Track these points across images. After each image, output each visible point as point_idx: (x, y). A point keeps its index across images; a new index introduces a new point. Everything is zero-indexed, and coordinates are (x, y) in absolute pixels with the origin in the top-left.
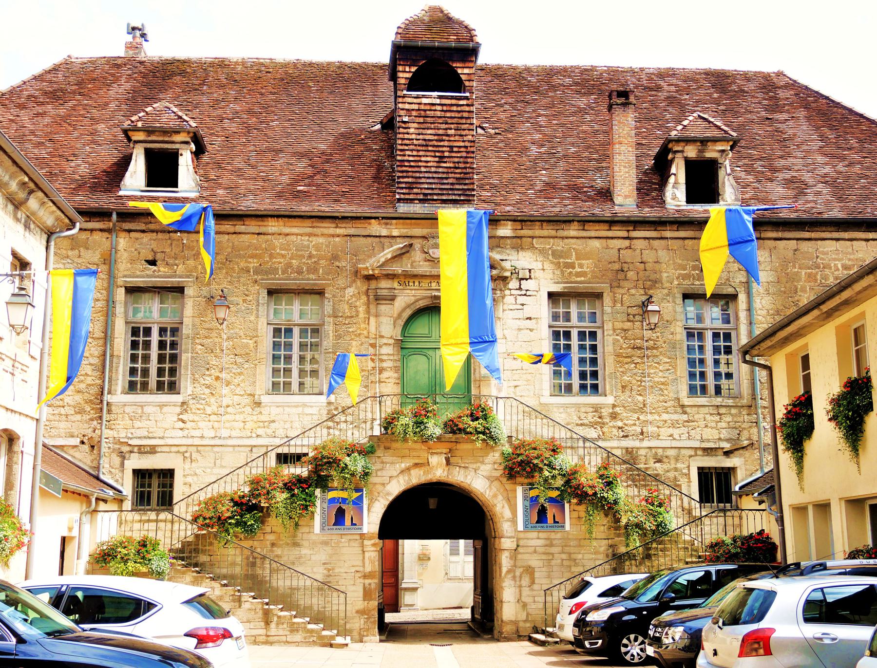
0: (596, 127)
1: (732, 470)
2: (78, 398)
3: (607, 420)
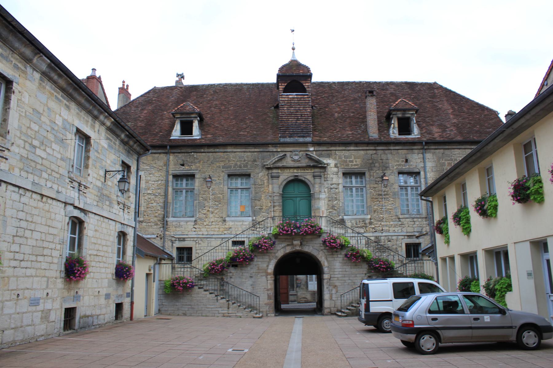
1: (419, 244)
3: (368, 225)
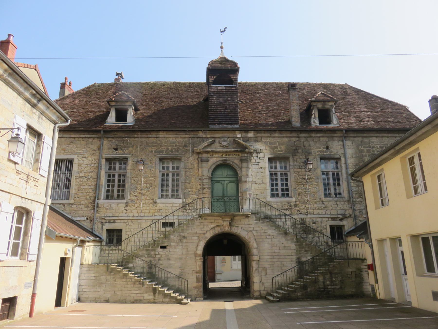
0: (283, 101)
1: (343, 226)
2: (86, 201)
3: (293, 207)
